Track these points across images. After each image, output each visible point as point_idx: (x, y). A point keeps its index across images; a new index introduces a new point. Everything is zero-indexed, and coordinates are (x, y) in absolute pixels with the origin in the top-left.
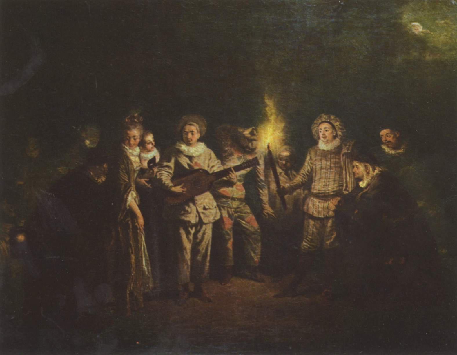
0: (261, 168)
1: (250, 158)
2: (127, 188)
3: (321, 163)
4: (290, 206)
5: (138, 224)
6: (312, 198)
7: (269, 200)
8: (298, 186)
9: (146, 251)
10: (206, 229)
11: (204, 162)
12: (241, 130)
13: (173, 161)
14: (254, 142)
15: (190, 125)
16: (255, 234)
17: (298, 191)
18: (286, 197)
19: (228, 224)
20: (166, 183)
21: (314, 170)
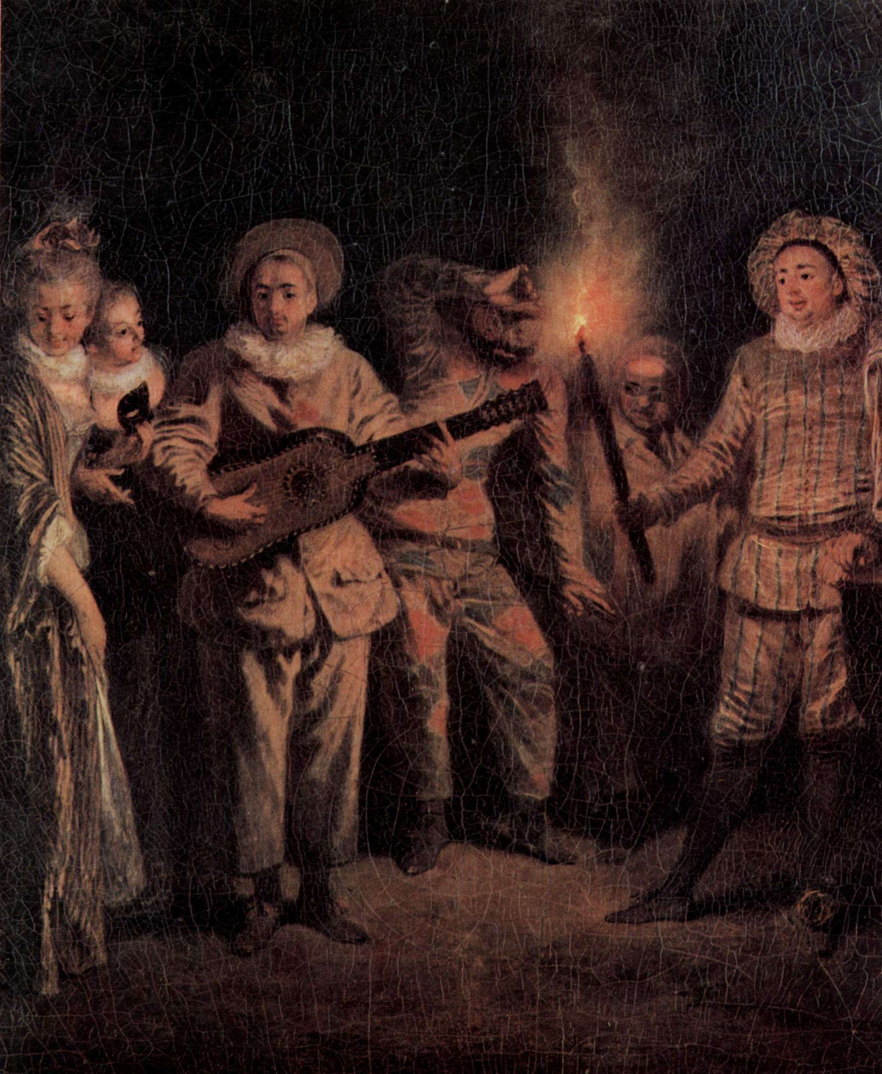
0: (554, 424)
1: (511, 383)
2: (39, 506)
3: (787, 400)
4: (667, 569)
5: (83, 642)
6: (754, 538)
7: (587, 546)
8: (700, 494)
9: (114, 746)
10: (343, 660)
11: (333, 405)
12: (477, 278)
13: (214, 399)
14: (524, 324)
15: (280, 258)
16: (532, 678)
17: (699, 510)
18: (652, 534)
19: (430, 646)
20: (189, 483)
21: (760, 431)
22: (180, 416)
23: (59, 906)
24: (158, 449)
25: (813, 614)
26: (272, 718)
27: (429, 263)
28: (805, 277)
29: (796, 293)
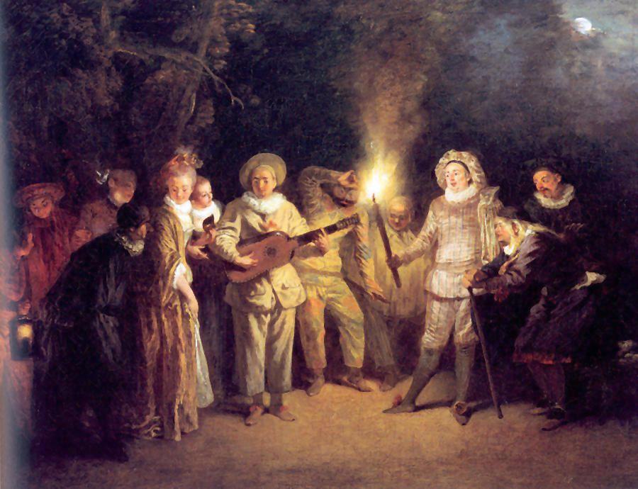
0: (363, 231)
8: (419, 253)
10: (286, 316)
13: (239, 219)
18: (400, 270)
20: (229, 251)
22: (226, 226)
23: (181, 408)
24: (218, 239)
25: (459, 299)
26: (259, 336)
27: (317, 169)
28: (456, 174)
29: (453, 180)
